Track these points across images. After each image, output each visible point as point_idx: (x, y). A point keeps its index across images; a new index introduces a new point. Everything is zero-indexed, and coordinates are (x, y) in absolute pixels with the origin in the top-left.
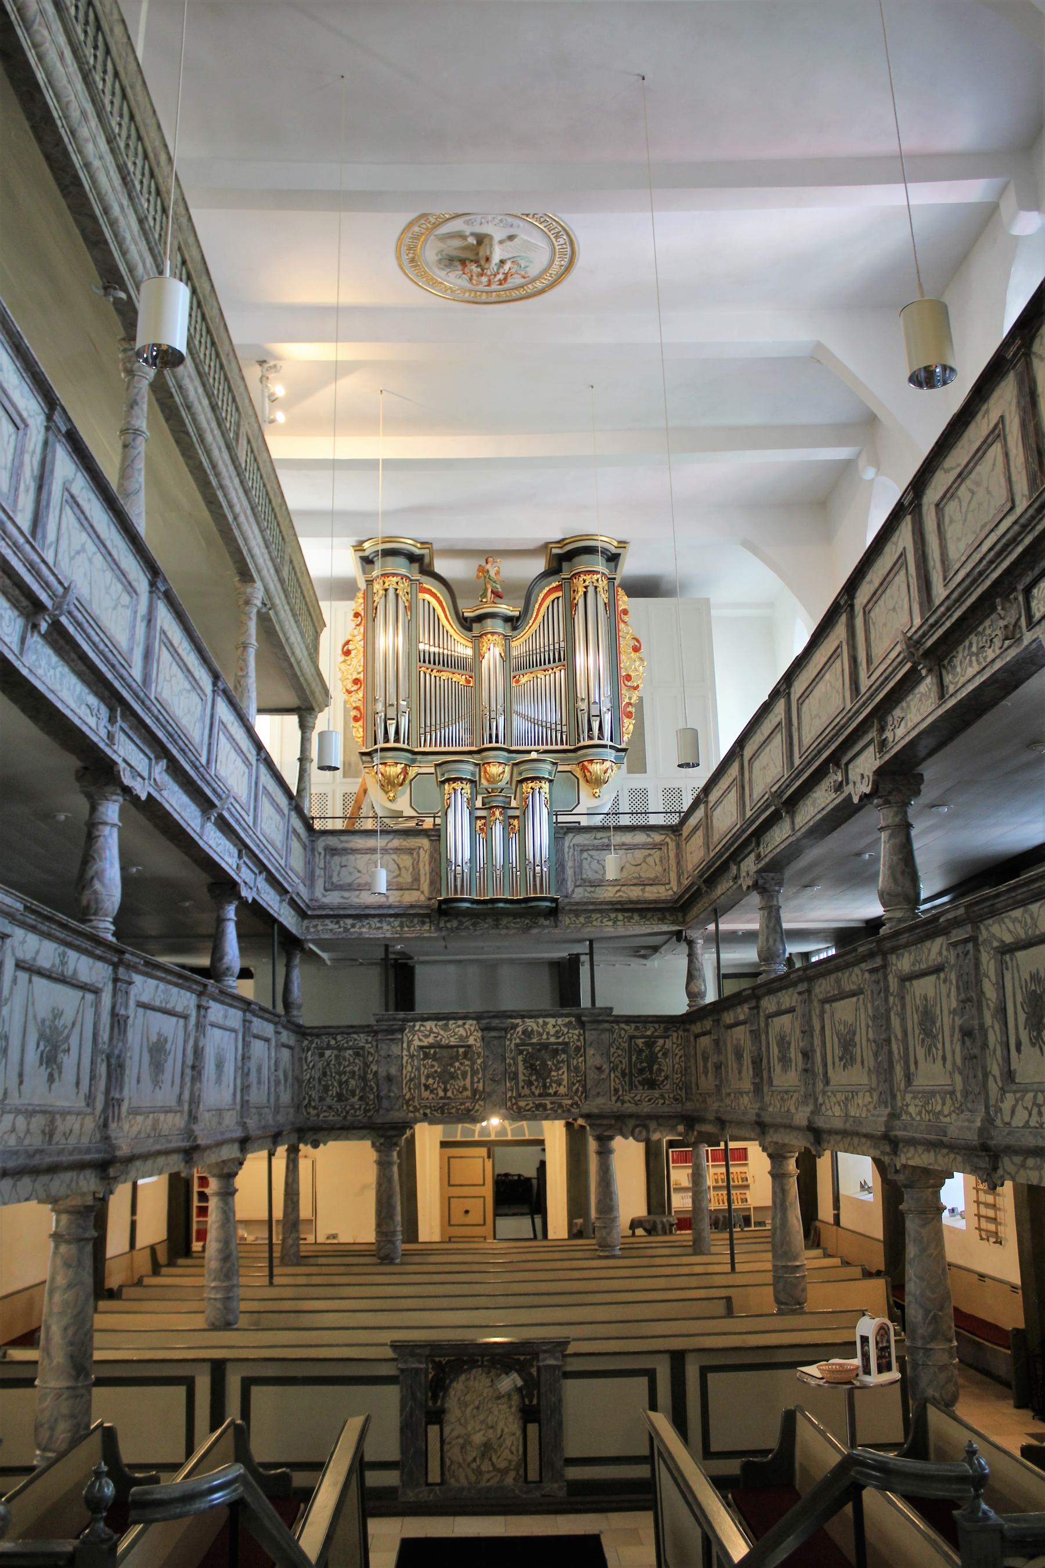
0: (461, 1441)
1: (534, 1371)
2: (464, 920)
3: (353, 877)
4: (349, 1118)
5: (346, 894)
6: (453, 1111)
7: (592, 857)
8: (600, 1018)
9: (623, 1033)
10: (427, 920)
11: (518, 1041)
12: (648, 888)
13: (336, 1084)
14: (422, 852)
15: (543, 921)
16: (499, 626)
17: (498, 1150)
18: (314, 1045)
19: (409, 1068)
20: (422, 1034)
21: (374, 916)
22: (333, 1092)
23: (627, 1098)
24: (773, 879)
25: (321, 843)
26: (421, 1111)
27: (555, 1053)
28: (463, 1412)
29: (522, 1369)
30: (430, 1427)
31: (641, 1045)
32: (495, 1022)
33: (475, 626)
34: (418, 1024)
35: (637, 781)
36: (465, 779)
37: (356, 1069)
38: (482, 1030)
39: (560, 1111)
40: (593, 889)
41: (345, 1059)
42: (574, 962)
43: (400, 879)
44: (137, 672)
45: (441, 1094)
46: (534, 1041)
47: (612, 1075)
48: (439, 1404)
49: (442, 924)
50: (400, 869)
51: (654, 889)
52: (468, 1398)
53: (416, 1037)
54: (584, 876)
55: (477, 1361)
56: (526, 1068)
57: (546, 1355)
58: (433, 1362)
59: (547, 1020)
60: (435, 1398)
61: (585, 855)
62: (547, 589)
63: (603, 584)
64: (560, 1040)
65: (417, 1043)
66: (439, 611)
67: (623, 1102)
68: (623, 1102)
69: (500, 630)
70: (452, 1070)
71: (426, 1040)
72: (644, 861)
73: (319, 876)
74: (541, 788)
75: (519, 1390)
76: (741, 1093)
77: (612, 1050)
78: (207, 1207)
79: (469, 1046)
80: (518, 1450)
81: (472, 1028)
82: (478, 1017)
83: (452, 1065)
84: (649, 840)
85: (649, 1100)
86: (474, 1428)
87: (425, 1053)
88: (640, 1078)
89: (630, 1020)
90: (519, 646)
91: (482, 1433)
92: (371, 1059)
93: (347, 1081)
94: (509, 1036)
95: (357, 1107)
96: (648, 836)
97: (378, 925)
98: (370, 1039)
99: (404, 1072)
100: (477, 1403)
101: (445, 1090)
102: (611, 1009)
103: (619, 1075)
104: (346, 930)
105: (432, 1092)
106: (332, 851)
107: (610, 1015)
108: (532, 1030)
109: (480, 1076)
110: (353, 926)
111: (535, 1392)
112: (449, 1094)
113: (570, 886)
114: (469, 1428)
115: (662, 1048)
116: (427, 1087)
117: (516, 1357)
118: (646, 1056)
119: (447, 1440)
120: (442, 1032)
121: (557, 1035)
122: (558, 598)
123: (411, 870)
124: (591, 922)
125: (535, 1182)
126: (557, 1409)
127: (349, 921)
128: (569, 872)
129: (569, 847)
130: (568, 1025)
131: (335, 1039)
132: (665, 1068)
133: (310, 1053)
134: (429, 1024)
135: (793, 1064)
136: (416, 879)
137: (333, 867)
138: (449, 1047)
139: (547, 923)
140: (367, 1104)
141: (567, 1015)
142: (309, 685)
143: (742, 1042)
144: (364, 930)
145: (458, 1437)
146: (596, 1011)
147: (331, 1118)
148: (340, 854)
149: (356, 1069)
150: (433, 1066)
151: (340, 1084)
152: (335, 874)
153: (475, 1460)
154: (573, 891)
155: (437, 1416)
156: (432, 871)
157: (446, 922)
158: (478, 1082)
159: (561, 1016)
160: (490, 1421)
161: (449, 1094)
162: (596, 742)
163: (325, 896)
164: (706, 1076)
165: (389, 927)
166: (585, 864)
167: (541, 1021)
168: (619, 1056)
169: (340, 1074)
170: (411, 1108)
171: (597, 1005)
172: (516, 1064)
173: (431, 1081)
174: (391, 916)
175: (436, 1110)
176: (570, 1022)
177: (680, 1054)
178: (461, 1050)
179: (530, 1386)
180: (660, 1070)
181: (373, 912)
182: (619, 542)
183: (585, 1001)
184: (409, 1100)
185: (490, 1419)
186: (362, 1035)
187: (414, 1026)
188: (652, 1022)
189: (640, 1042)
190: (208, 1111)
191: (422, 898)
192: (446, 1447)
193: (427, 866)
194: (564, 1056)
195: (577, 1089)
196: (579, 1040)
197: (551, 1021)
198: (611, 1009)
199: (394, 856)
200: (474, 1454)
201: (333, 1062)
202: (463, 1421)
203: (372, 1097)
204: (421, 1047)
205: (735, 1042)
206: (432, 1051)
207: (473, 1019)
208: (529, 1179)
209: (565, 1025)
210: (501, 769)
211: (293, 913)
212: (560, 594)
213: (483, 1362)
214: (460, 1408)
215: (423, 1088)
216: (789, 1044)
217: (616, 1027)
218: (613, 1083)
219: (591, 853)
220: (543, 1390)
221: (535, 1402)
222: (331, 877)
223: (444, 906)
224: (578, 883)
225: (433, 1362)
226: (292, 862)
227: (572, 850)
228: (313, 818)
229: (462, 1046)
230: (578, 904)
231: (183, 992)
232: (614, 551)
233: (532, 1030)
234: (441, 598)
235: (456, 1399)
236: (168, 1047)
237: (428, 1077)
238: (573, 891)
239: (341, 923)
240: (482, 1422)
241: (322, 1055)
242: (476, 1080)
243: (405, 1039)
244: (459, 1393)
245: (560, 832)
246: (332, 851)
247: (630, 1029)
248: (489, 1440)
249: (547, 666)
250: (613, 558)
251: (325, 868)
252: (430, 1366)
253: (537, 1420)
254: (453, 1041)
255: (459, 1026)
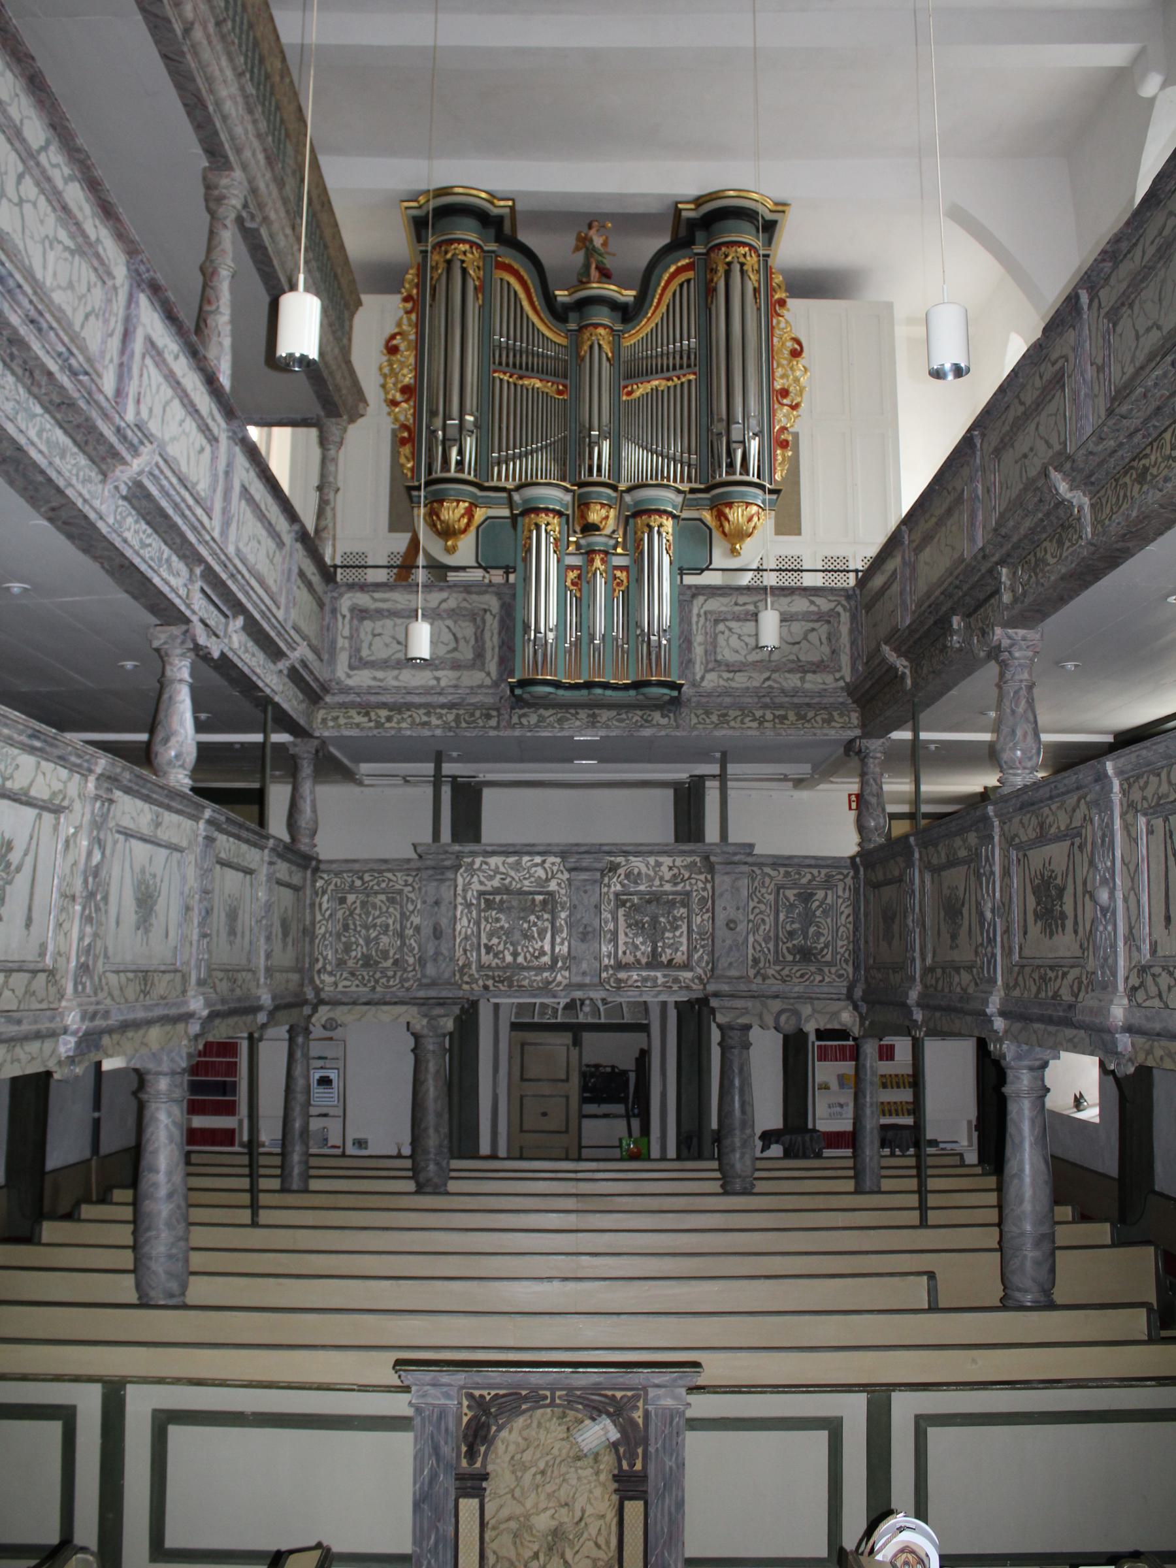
0: (513, 1525)
1: (638, 1416)
2: (546, 713)
3: (390, 651)
4: (378, 989)
5: (380, 674)
6: (526, 983)
7: (730, 629)
8: (736, 858)
9: (767, 880)
10: (494, 713)
11: (619, 887)
12: (809, 676)
13: (361, 941)
14: (488, 617)
15: (657, 716)
16: (603, 317)
17: (587, 1037)
18: (332, 887)
19: (465, 922)
20: (483, 873)
21: (419, 706)
22: (357, 953)
23: (770, 972)
24: (1024, 639)
25: (346, 602)
26: (481, 983)
27: (672, 904)
28: (518, 1480)
29: (617, 1410)
30: (463, 1502)
31: (792, 899)
32: (586, 861)
33: (572, 316)
34: (478, 861)
35: (789, 546)
36: (553, 511)
37: (390, 921)
38: (570, 870)
39: (675, 987)
40: (731, 675)
41: (374, 906)
42: (698, 783)
43: (456, 655)
44: (108, 384)
45: (509, 959)
46: (642, 888)
47: (751, 939)
48: (478, 1465)
49: (515, 720)
50: (456, 639)
51: (818, 678)
52: (527, 1456)
53: (475, 879)
54: (719, 657)
55: (545, 1398)
56: (629, 926)
57: (661, 1391)
58: (470, 1396)
59: (661, 859)
60: (471, 1455)
61: (721, 627)
62: (672, 269)
63: (752, 260)
64: (679, 888)
65: (476, 886)
66: (522, 295)
67: (765, 978)
68: (765, 978)
69: (606, 322)
70: (526, 926)
71: (489, 884)
72: (805, 638)
73: (343, 649)
74: (660, 526)
75: (615, 1445)
76: (957, 970)
77: (751, 904)
78: (194, 1108)
79: (551, 894)
80: (608, 1543)
81: (555, 868)
82: (563, 854)
83: (525, 919)
84: (813, 608)
85: (802, 976)
86: (536, 1505)
87: (487, 901)
88: (790, 945)
89: (778, 862)
90: (637, 336)
91: (550, 1513)
92: (411, 907)
93: (377, 938)
94: (606, 880)
95: (390, 974)
96: (812, 603)
97: (425, 719)
98: (410, 879)
99: (458, 927)
100: (542, 1465)
101: (515, 954)
102: (752, 846)
103: (760, 939)
104: (379, 725)
105: (496, 955)
106: (361, 614)
107: (750, 854)
108: (639, 873)
109: (564, 935)
110: (389, 719)
111: (640, 1451)
112: (520, 959)
113: (698, 669)
114: (529, 1504)
115: (822, 903)
116: (489, 949)
117: (610, 1393)
118: (799, 914)
119: (492, 1522)
120: (512, 873)
121: (674, 880)
122: (688, 281)
123: (473, 642)
124: (728, 722)
125: (632, 1076)
126: (674, 1479)
127: (384, 713)
128: (698, 651)
129: (699, 615)
130: (691, 867)
131: (361, 878)
132: (825, 932)
133: (326, 898)
134: (494, 861)
135: (1069, 923)
136: (480, 655)
137: (362, 635)
138: (520, 892)
139: (665, 721)
140: (405, 970)
141: (691, 853)
142: (331, 373)
143: (961, 893)
144: (404, 725)
145: (509, 1519)
146: (730, 849)
147: (354, 989)
148: (371, 618)
149: (390, 921)
150: (498, 920)
151: (368, 941)
152: (365, 645)
153: (536, 1556)
154: (703, 678)
155: (473, 1484)
156: (502, 644)
157: (520, 717)
158: (562, 943)
159: (683, 853)
160: (563, 1494)
161: (520, 959)
162: (738, 477)
163: (349, 676)
164: (890, 944)
165: (439, 722)
166: (721, 640)
167: (652, 860)
168: (761, 912)
169: (366, 927)
170: (466, 978)
171: (731, 840)
172: (615, 919)
173: (495, 941)
174: (442, 706)
175: (502, 982)
176: (694, 863)
177: (847, 912)
178: (539, 898)
179: (632, 1439)
180: (819, 934)
181: (417, 699)
182: (776, 204)
183: (712, 833)
184: (464, 966)
185: (562, 1491)
186: (399, 874)
187: (473, 863)
188: (810, 866)
189: (791, 894)
190: (117, 972)
191: (488, 682)
192: (488, 1536)
193: (496, 639)
194: (682, 910)
195: (701, 957)
196: (704, 889)
197: (667, 861)
198: (752, 846)
199: (449, 622)
200: (536, 1547)
201: (358, 911)
202: (517, 1493)
203: (411, 960)
204: (481, 893)
205: (946, 892)
206: (498, 898)
207: (555, 854)
208: (625, 1073)
209: (685, 867)
210: (603, 512)
211: (301, 696)
212: (690, 274)
213: (553, 1399)
214: (513, 1472)
215: (483, 951)
216: (1061, 891)
217: (758, 872)
218: (751, 951)
219: (729, 624)
220: (651, 1449)
221: (638, 1466)
222: (358, 650)
223: (518, 692)
224: (711, 666)
225: (470, 1396)
226: (290, 609)
227: (702, 620)
228: (335, 567)
229: (540, 893)
230: (709, 695)
231: (47, 766)
232: (770, 217)
233: (639, 873)
234: (526, 277)
235: (507, 1458)
236: (15, 857)
237: (491, 936)
238: (703, 678)
239: (373, 715)
240: (549, 1496)
241: (343, 901)
242: (558, 940)
243: (460, 881)
244: (512, 1448)
245: (685, 597)
246: (361, 614)
247: (779, 875)
248: (561, 1524)
249: (671, 374)
250: (769, 228)
251: (351, 638)
252: (465, 1403)
253: (642, 1496)
254: (527, 885)
255: (536, 865)
